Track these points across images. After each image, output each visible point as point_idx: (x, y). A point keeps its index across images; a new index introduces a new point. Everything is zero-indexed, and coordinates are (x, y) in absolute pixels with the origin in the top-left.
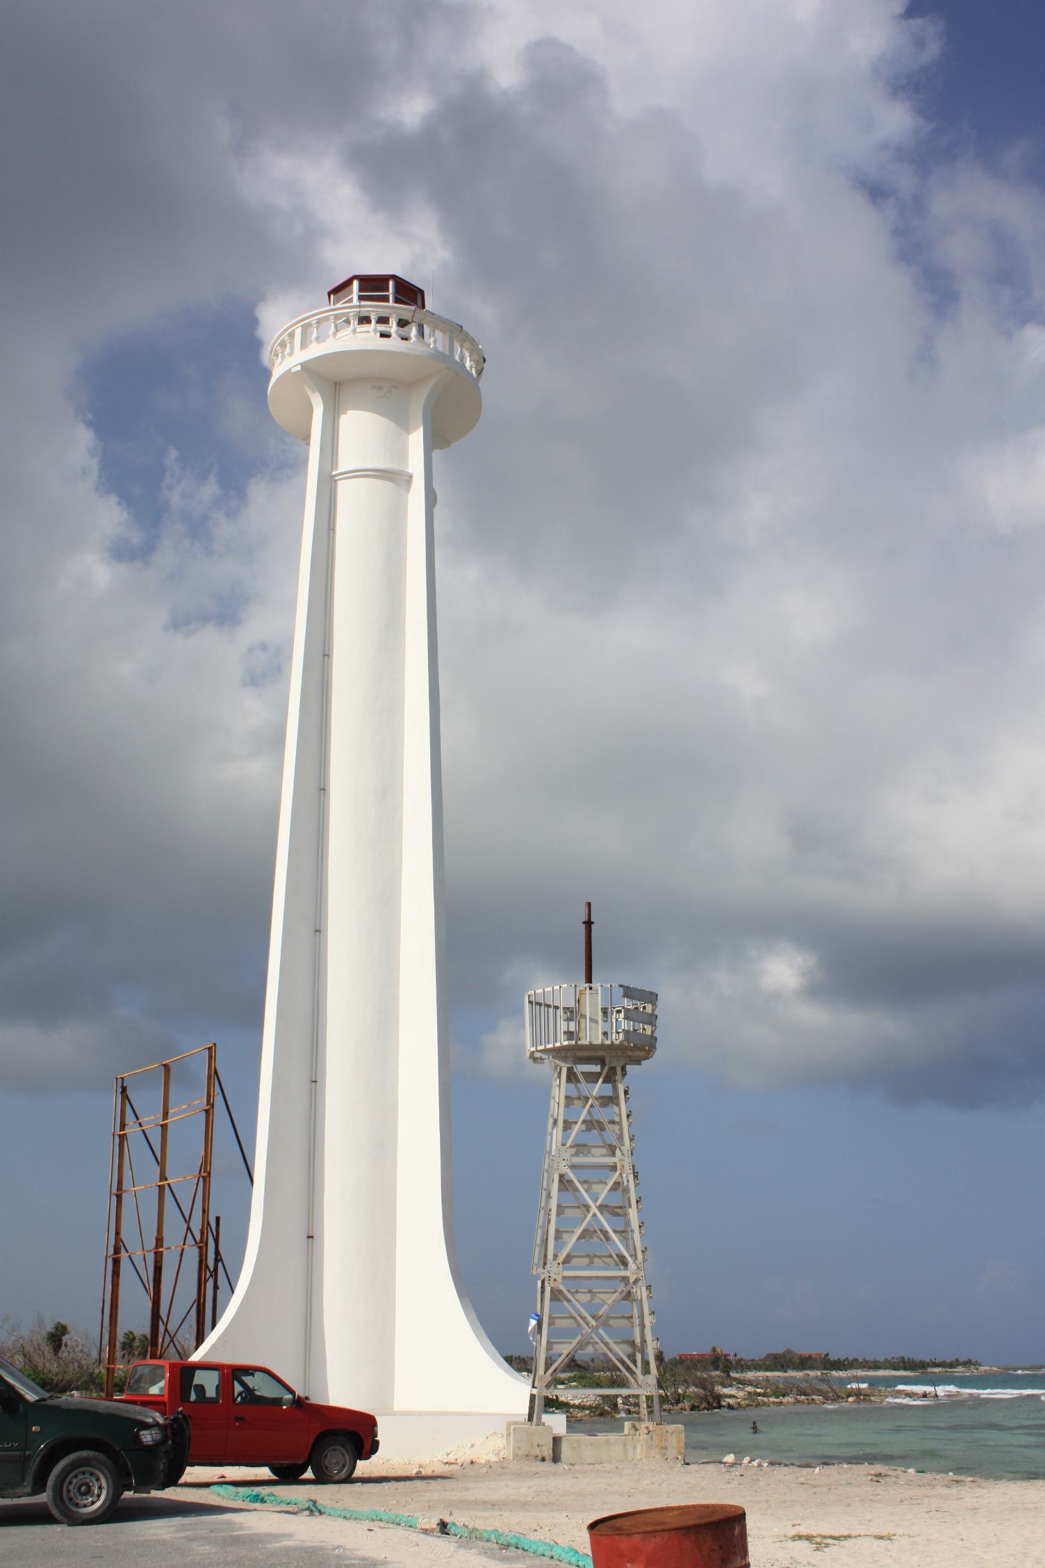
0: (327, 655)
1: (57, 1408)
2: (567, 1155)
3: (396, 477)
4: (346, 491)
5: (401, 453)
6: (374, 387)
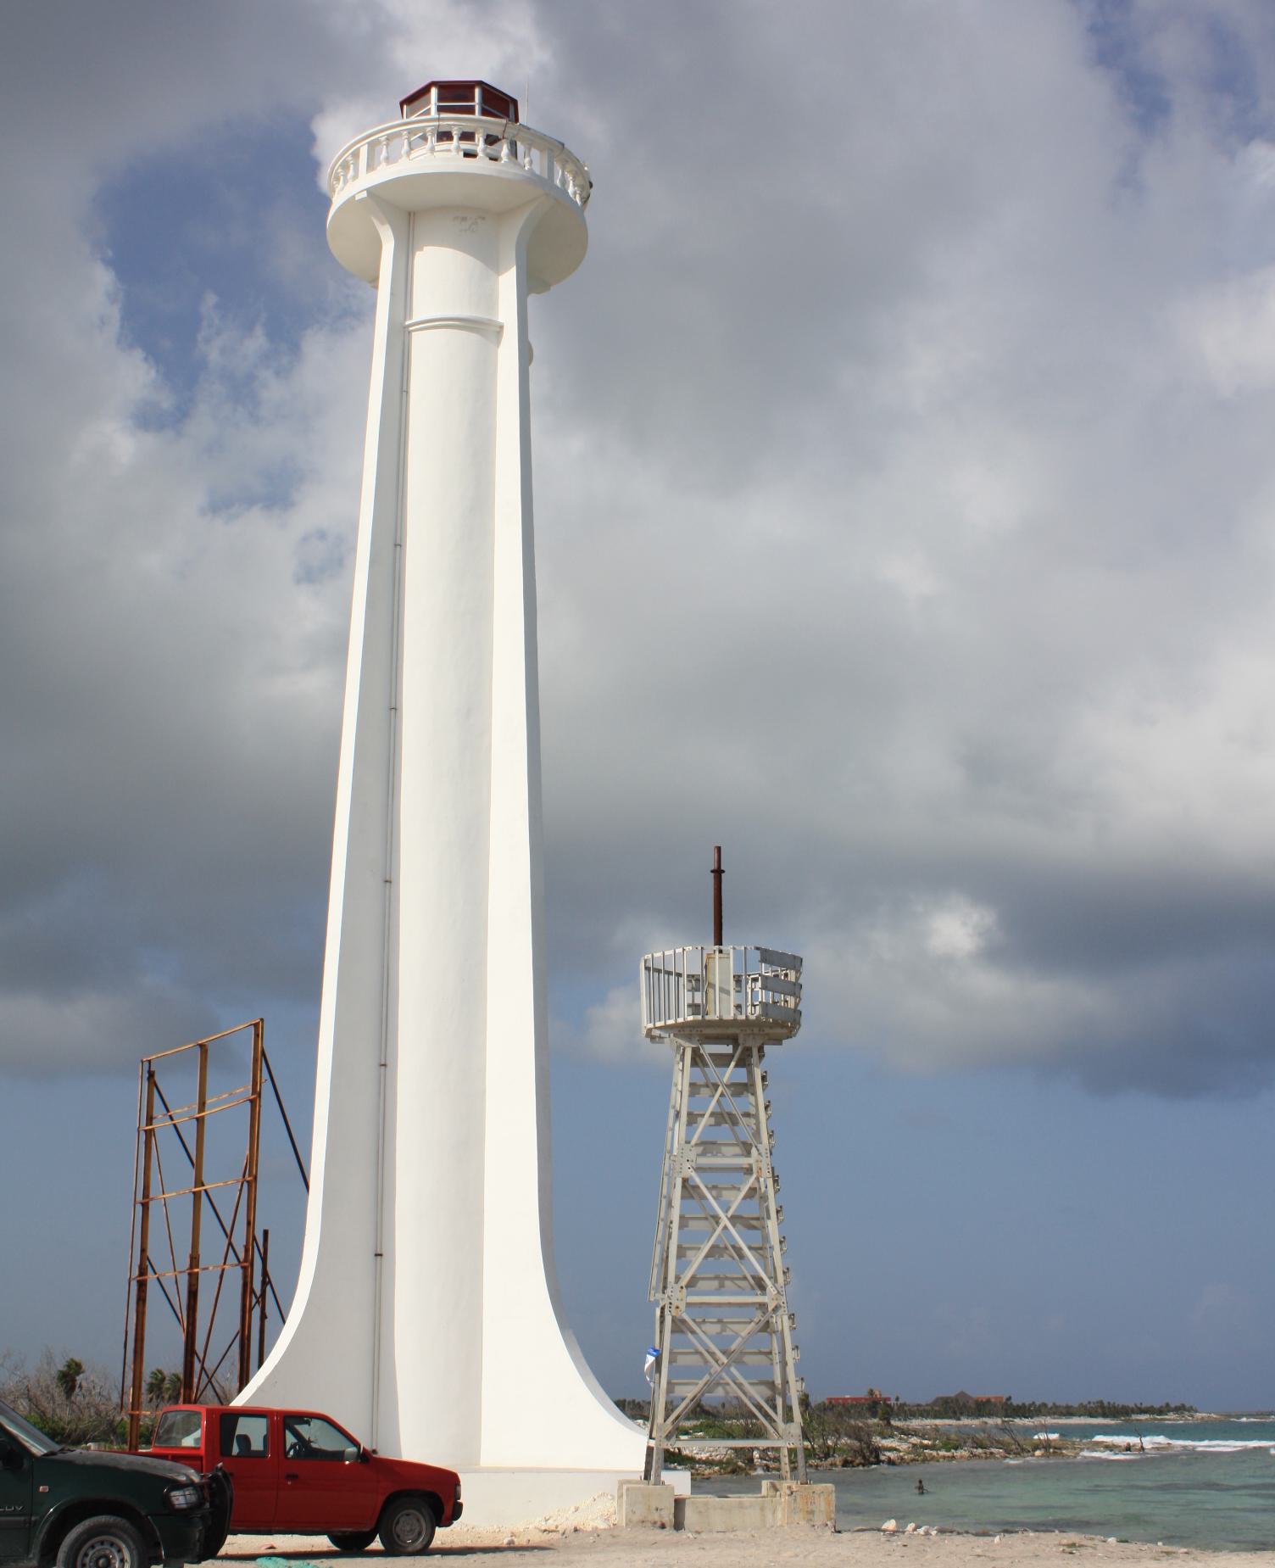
0: (398, 545)
1: (70, 1464)
3: (483, 328)
5: (490, 298)
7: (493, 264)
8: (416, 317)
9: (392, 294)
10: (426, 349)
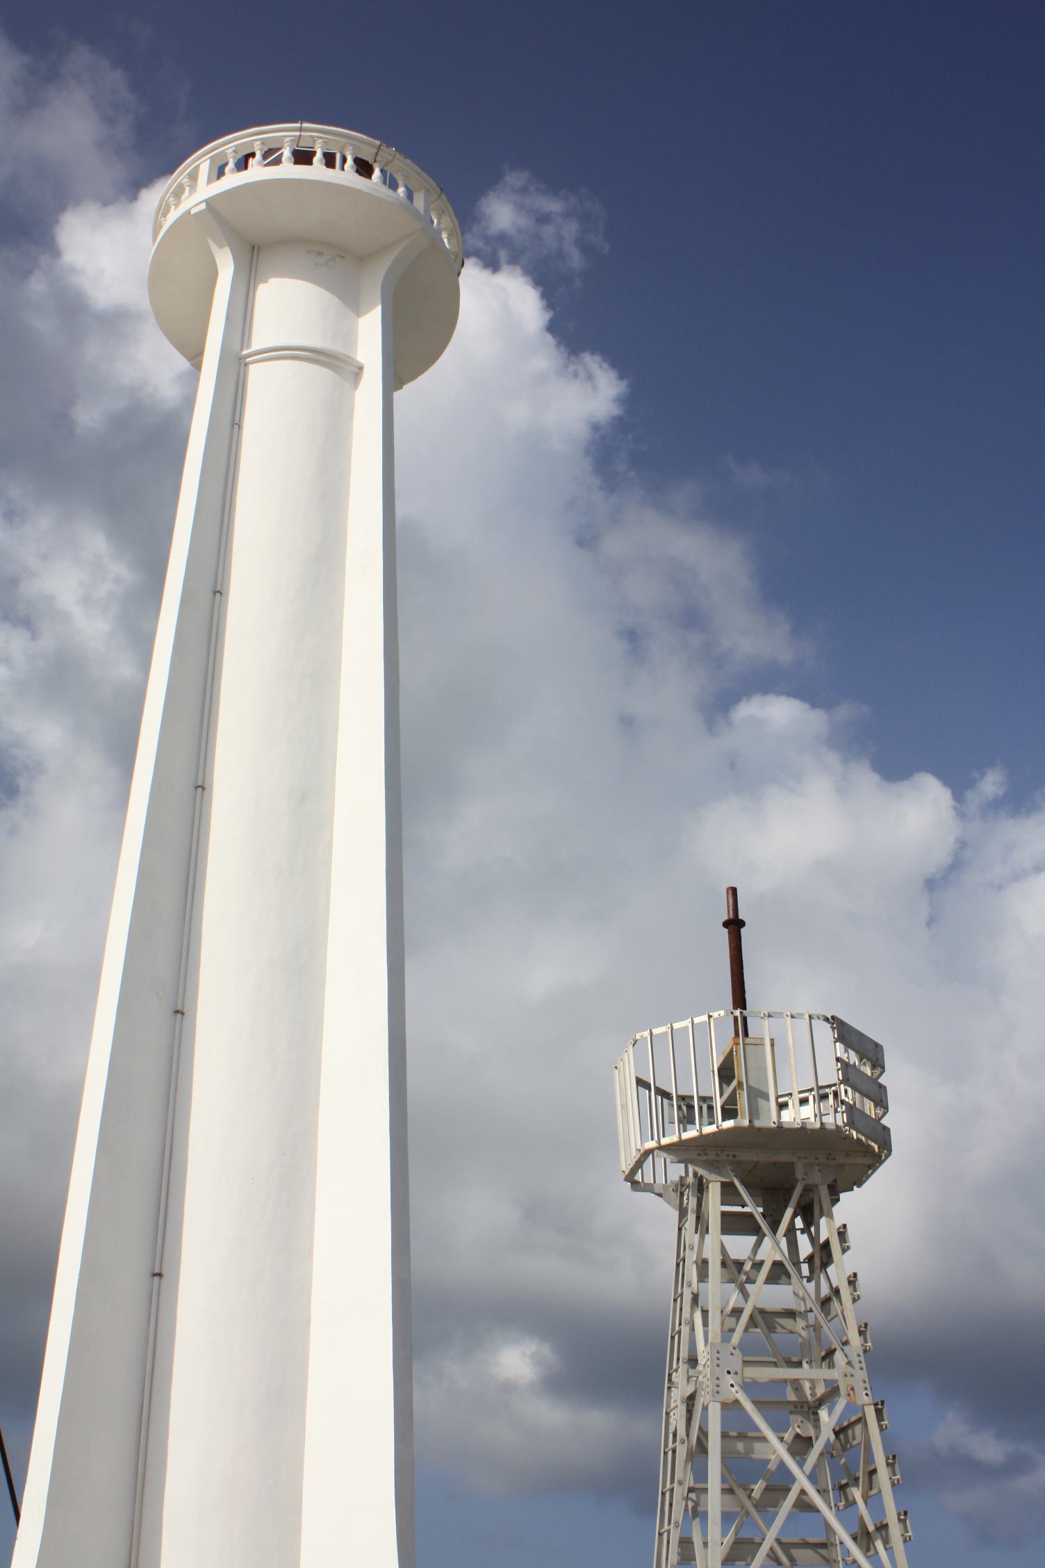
0: (219, 593)
1: (859, 1071)
2: (736, 1361)
3: (336, 362)
4: (259, 377)
5: (350, 337)
6: (309, 252)
7: (353, 303)
8: (257, 344)
9: (228, 318)
10: (263, 381)
